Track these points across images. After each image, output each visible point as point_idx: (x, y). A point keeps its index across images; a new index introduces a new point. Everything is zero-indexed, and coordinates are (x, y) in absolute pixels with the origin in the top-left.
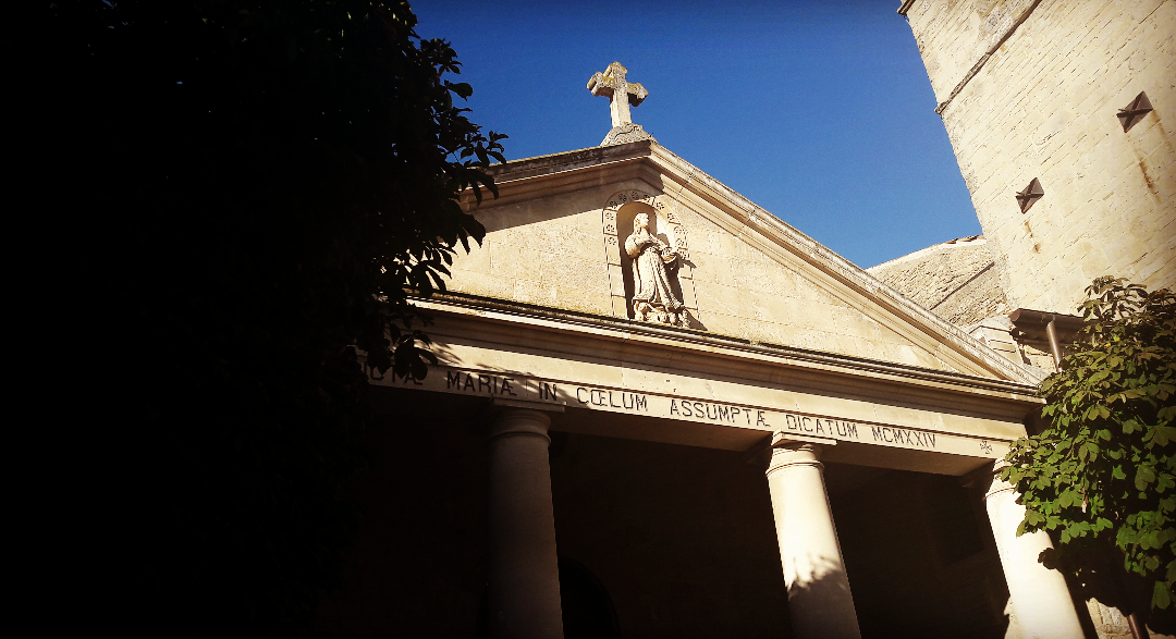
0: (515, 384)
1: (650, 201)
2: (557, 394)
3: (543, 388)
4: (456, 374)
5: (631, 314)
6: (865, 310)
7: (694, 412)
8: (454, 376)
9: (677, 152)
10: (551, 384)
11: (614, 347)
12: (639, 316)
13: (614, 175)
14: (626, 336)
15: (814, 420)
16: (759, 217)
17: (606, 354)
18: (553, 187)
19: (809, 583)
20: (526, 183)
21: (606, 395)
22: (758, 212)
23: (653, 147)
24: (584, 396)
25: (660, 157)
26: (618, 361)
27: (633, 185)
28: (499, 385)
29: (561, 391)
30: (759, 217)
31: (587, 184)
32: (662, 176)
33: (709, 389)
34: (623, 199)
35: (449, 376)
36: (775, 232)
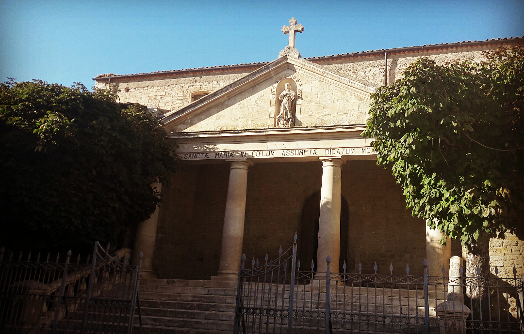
4: (217, 154)
7: (290, 153)
11: (265, 137)
24: (254, 154)
27: (285, 72)
31: (267, 78)
32: (295, 66)
34: (280, 79)
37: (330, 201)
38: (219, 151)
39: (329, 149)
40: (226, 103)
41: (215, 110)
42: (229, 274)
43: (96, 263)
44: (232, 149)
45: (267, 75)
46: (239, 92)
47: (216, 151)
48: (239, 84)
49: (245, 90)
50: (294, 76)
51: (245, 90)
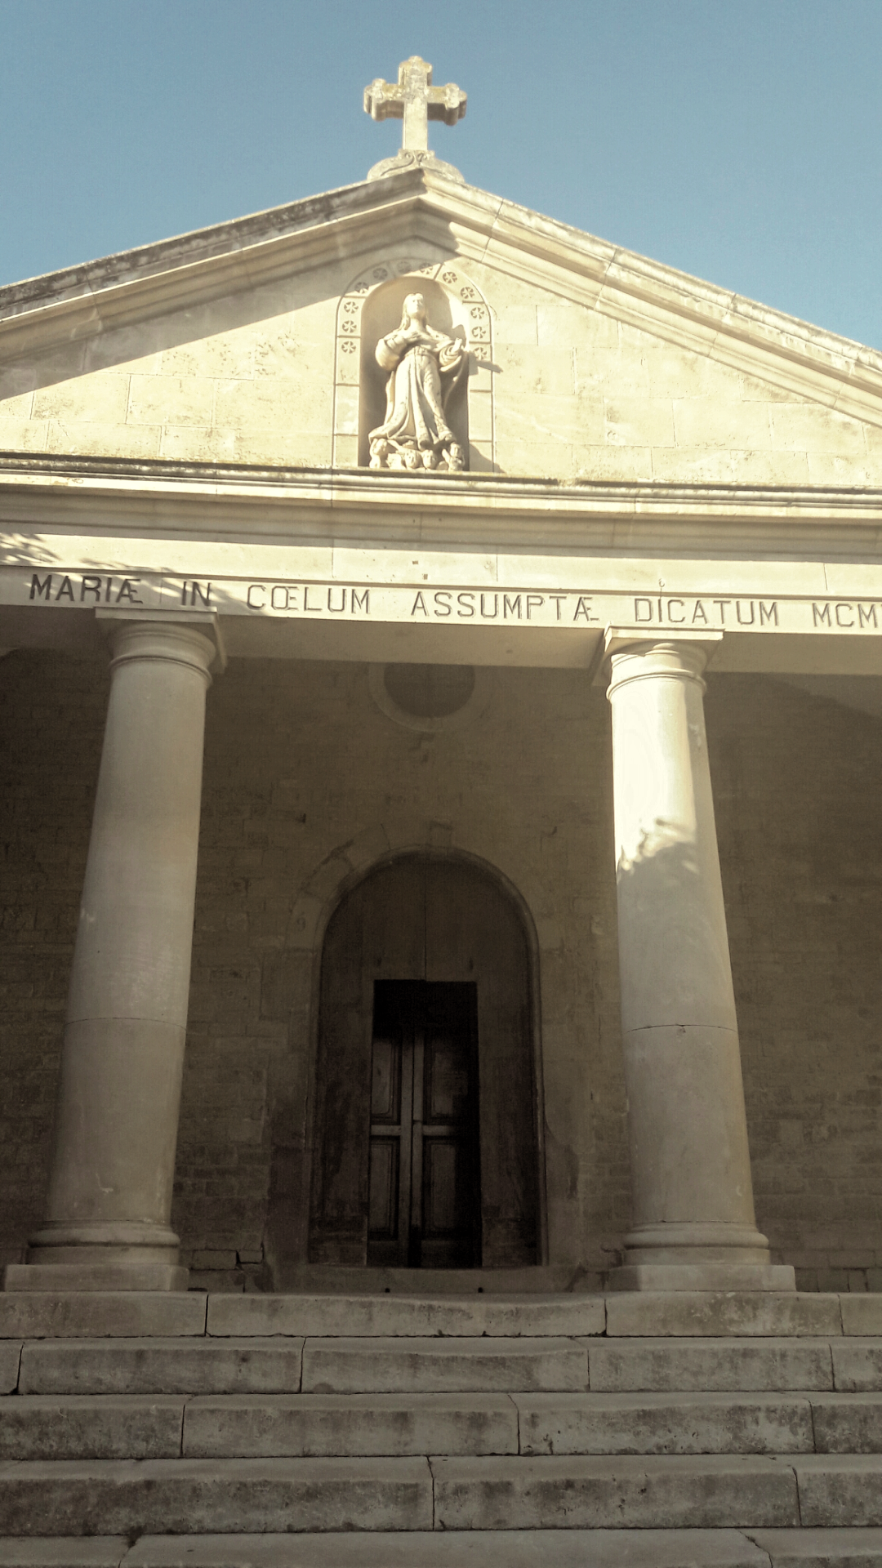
0: (143, 587)
1: (429, 273)
2: (212, 597)
3: (189, 588)
4: (42, 578)
5: (365, 459)
6: (839, 404)
7: (455, 606)
8: (42, 580)
9: (476, 177)
10: (204, 583)
11: (319, 517)
12: (375, 464)
13: (364, 238)
14: (326, 495)
15: (691, 603)
16: (624, 267)
17: (306, 529)
18: (248, 275)
19: (635, 864)
20: (195, 274)
21: (298, 593)
22: (621, 259)
23: (428, 179)
24: (259, 598)
25: (442, 193)
26: (328, 539)
27: (402, 250)
28: (115, 589)
29: (222, 594)
30: (624, 267)
31: (315, 261)
32: (453, 227)
33: (491, 567)
34: (380, 274)
35: (35, 581)
36: (655, 290)
37: (689, 838)
38: (57, 564)
39: (654, 599)
40: (95, 346)
41: (31, 372)
42: (124, 1246)
43: (859, 1291)
44: (135, 563)
45: (315, 246)
46: (165, 306)
47: (35, 563)
48: (175, 262)
49: (200, 303)
50: (445, 270)
51: (200, 303)
